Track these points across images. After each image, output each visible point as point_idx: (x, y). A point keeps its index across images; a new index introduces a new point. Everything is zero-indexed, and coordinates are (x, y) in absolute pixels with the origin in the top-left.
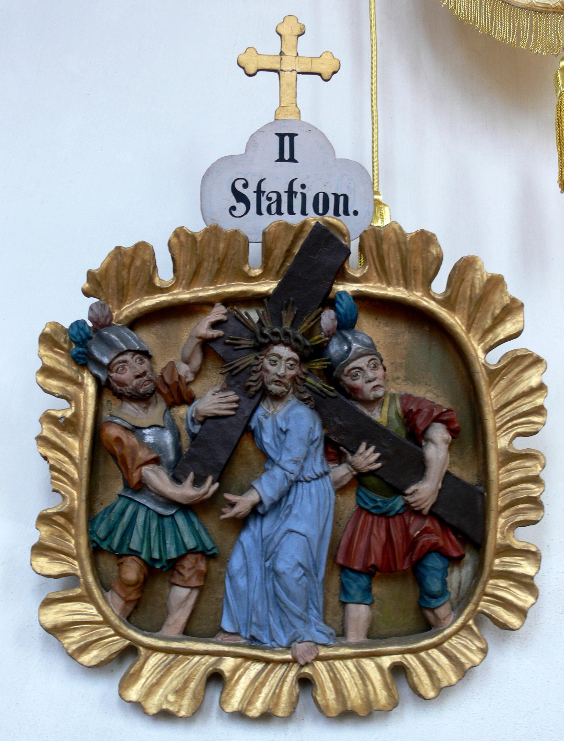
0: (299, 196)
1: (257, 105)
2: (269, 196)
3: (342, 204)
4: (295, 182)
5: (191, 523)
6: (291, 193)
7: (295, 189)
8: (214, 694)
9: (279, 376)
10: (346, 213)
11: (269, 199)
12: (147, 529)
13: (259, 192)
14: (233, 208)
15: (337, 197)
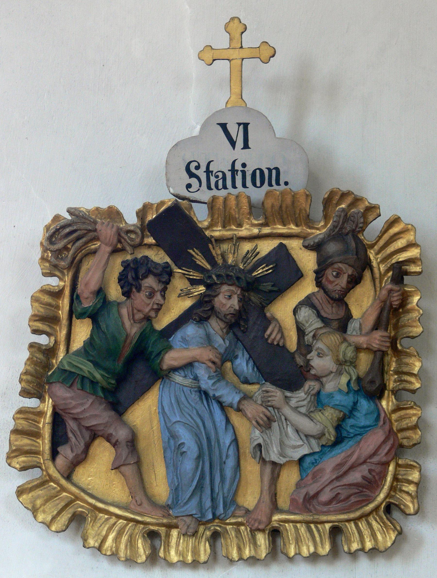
0: (240, 173)
6: (233, 171)
7: (236, 168)
8: (396, 514)
10: (278, 183)
11: (217, 177)
12: (235, 483)
13: (208, 172)
14: (189, 186)
15: (270, 170)
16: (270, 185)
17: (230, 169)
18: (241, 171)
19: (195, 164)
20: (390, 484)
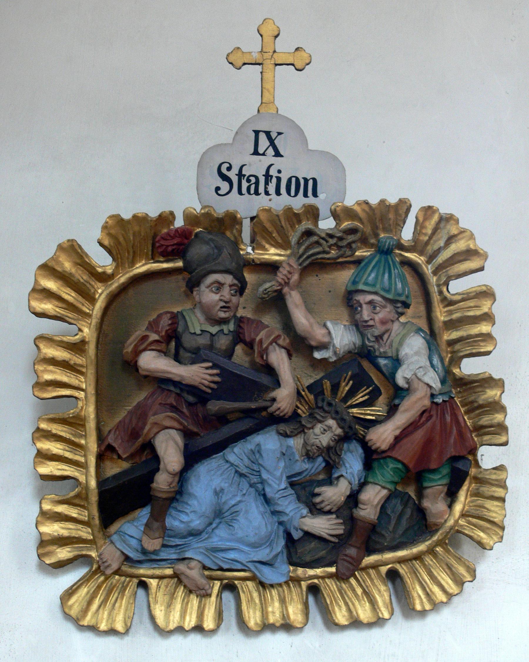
0: (274, 180)
1: (238, 100)
2: (251, 178)
3: (308, 186)
4: (244, 168)
5: (359, 573)
6: (268, 177)
9: (226, 302)
10: (315, 194)
11: (248, 181)
13: (240, 175)
14: (218, 189)
15: (306, 180)
16: (306, 195)
17: (237, 173)
18: (276, 177)
19: (226, 165)
20: (425, 595)
